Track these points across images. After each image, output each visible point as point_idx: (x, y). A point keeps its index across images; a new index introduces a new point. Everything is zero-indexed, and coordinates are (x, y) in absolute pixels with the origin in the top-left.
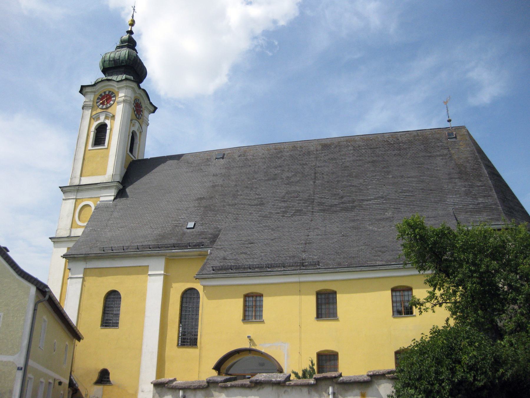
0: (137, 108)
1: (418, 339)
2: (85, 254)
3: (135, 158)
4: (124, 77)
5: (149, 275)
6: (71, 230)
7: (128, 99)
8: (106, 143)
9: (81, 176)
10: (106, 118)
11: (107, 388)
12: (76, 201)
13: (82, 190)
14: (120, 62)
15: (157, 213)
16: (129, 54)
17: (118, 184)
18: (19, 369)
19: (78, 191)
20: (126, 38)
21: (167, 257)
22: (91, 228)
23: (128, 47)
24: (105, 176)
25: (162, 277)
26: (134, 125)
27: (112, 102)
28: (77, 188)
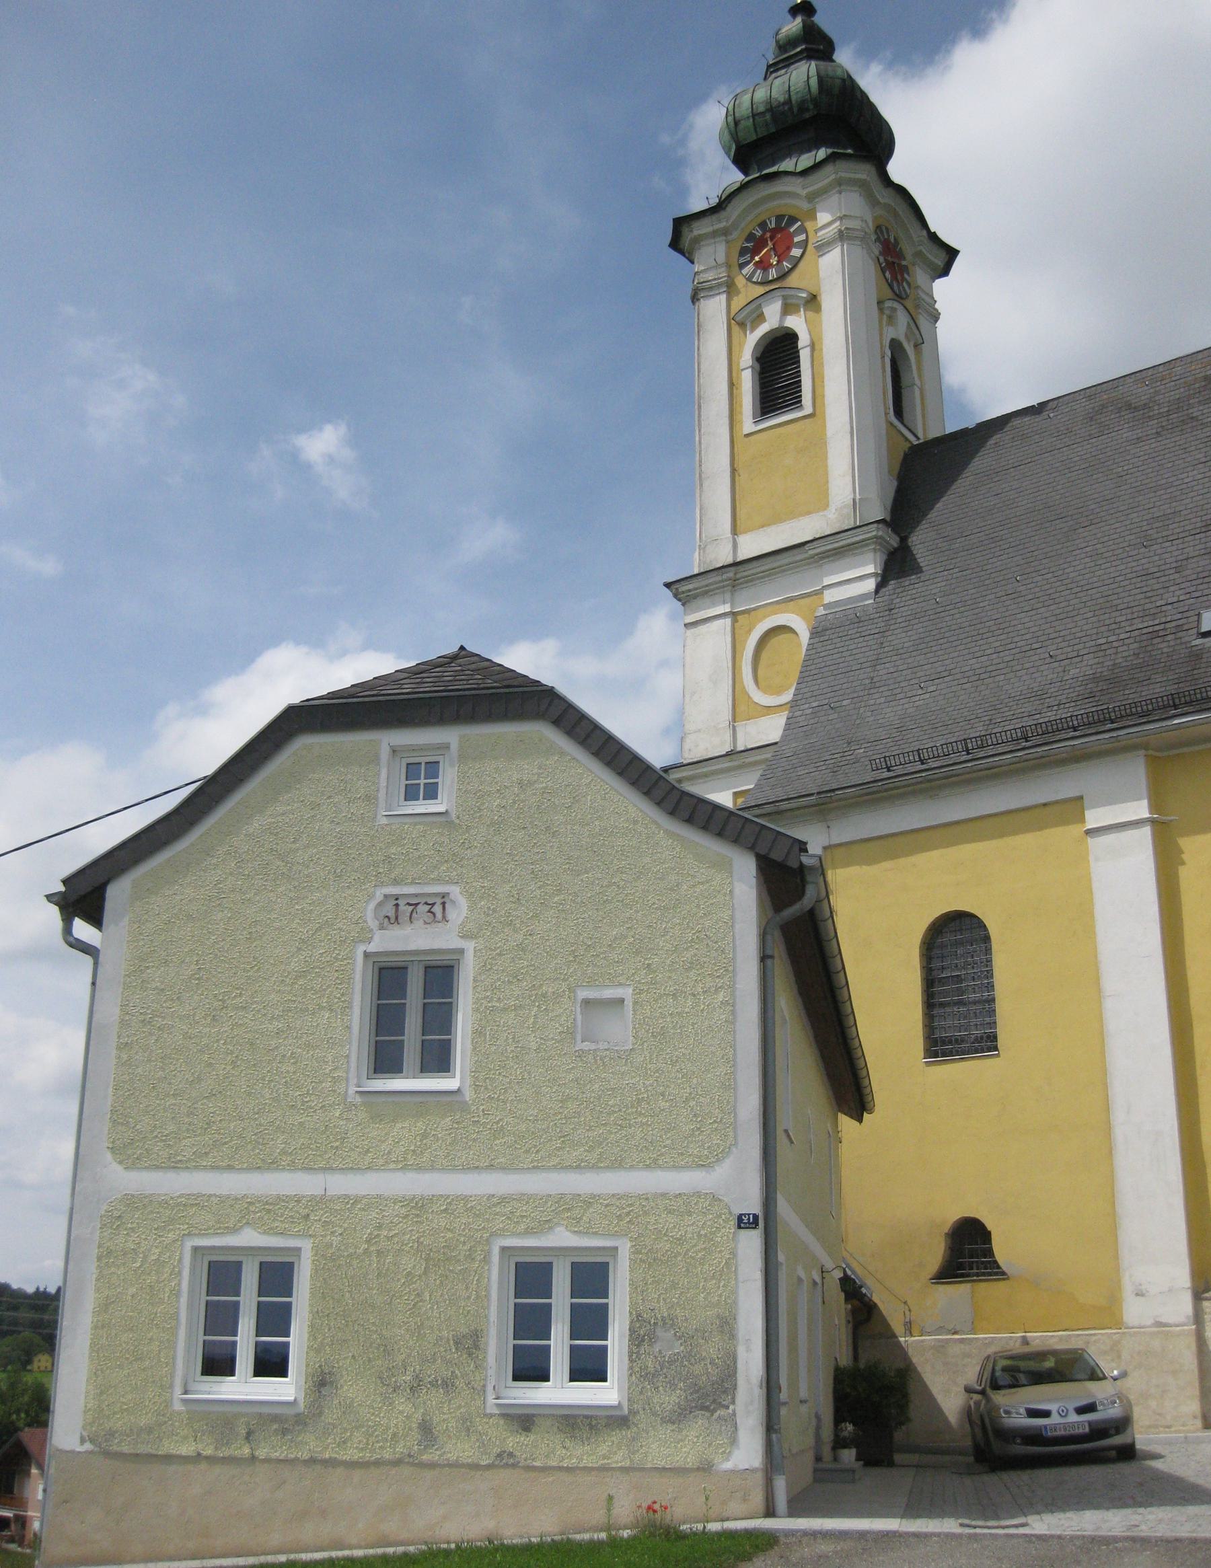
0: (889, 258)
1: (42, 1289)
2: (819, 793)
3: (918, 439)
4: (822, 153)
5: (1089, 832)
6: (734, 727)
7: (855, 224)
8: (803, 393)
9: (735, 531)
10: (787, 309)
11: (988, 1290)
12: (734, 621)
13: (751, 581)
14: (795, 110)
15: (1062, 605)
16: (823, 73)
17: (882, 531)
18: (745, 1222)
19: (735, 585)
20: (794, 29)
21: (1150, 752)
22: (815, 704)
23: (810, 55)
24: (826, 512)
25: (1147, 831)
26: (891, 320)
27: (796, 252)
28: (730, 574)
